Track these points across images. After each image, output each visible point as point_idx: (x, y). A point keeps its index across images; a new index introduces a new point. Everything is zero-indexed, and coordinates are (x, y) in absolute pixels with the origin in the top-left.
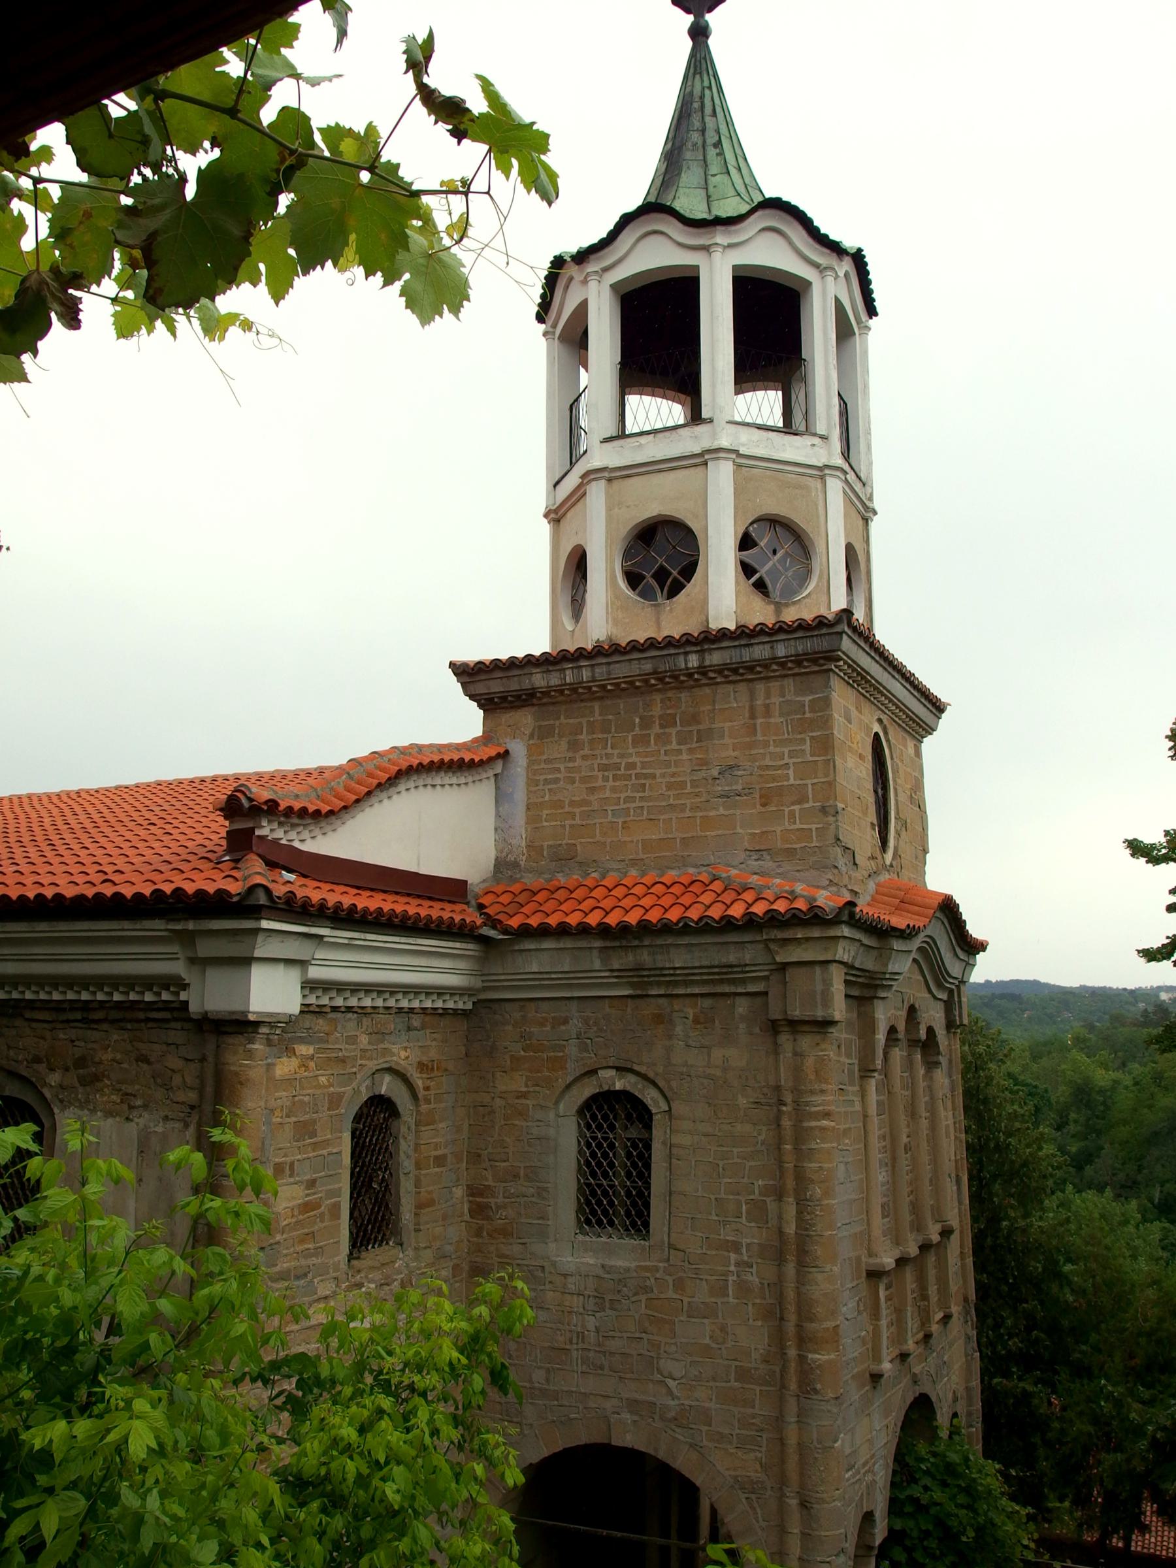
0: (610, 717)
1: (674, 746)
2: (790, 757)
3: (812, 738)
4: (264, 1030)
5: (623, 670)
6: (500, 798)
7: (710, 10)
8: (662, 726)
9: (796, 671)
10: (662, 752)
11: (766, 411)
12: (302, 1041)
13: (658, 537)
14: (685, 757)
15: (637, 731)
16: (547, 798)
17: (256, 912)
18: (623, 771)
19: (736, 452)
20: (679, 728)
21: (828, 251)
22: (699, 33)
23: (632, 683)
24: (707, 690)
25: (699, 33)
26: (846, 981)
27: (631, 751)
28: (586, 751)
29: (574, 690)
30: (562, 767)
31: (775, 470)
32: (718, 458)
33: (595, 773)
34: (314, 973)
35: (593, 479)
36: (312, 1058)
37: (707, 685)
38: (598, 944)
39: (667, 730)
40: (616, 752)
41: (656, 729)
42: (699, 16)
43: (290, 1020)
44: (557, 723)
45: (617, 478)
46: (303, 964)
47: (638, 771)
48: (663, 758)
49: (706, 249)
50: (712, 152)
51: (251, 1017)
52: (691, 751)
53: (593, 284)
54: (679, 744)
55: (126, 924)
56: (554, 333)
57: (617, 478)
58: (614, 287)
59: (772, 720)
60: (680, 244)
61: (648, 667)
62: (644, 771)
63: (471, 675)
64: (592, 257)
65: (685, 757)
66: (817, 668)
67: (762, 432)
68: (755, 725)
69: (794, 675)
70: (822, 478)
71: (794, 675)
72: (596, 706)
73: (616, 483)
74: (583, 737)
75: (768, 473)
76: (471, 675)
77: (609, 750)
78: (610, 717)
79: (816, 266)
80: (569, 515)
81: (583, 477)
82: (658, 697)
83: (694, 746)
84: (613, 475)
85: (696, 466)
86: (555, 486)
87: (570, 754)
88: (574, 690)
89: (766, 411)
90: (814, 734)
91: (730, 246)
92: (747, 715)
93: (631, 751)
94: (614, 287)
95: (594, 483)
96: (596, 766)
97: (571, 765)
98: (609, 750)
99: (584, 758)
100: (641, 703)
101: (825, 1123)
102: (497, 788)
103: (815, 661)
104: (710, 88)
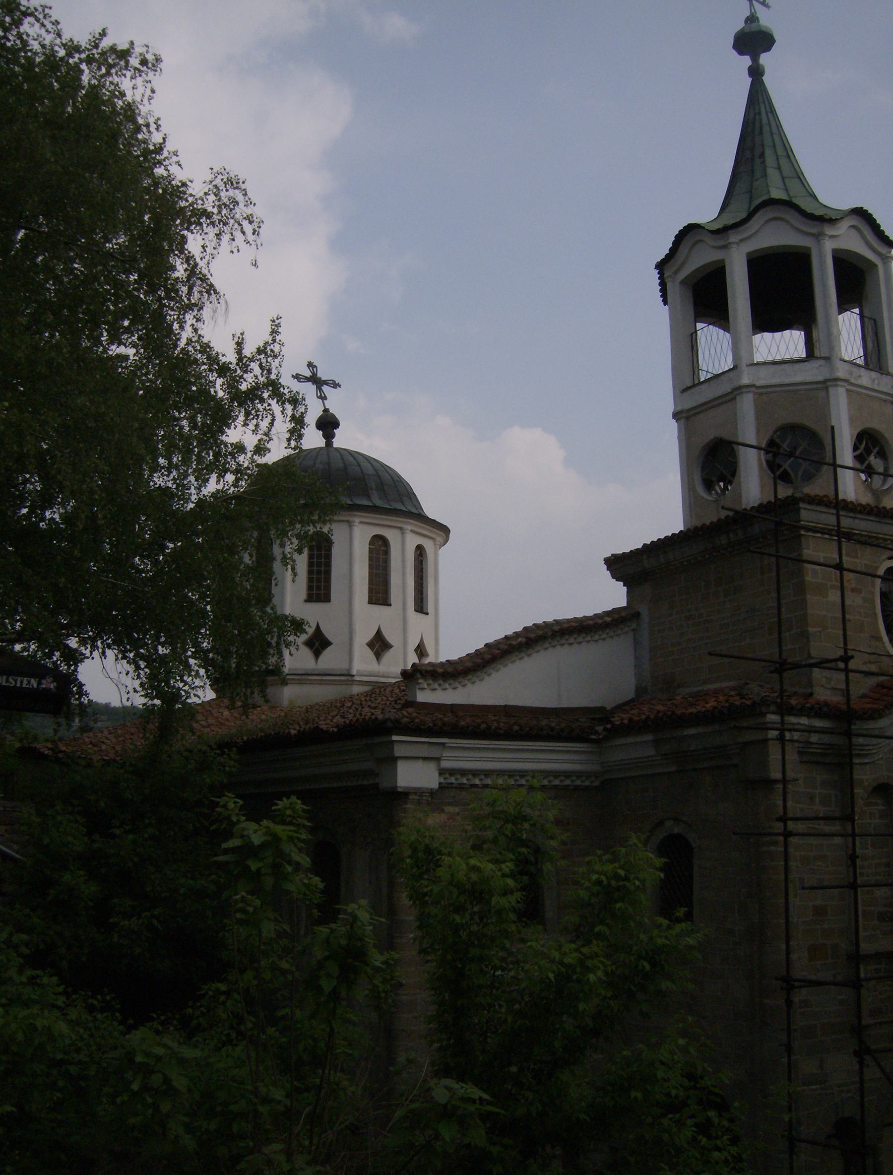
4: (411, 797)
6: (637, 643)
11: (792, 347)
12: (450, 804)
16: (659, 642)
17: (390, 732)
19: (753, 386)
22: (756, 72)
25: (756, 72)
26: (799, 753)
32: (741, 393)
34: (445, 764)
36: (458, 814)
38: (649, 737)
42: (755, 59)
43: (432, 793)
45: (691, 416)
46: (438, 760)
50: (758, 161)
51: (399, 790)
55: (530, 743)
58: (684, 282)
60: (714, 247)
63: (617, 565)
67: (777, 366)
70: (827, 388)
76: (617, 565)
79: (813, 235)
89: (792, 347)
91: (741, 241)
101: (773, 848)
102: (635, 639)
104: (760, 113)
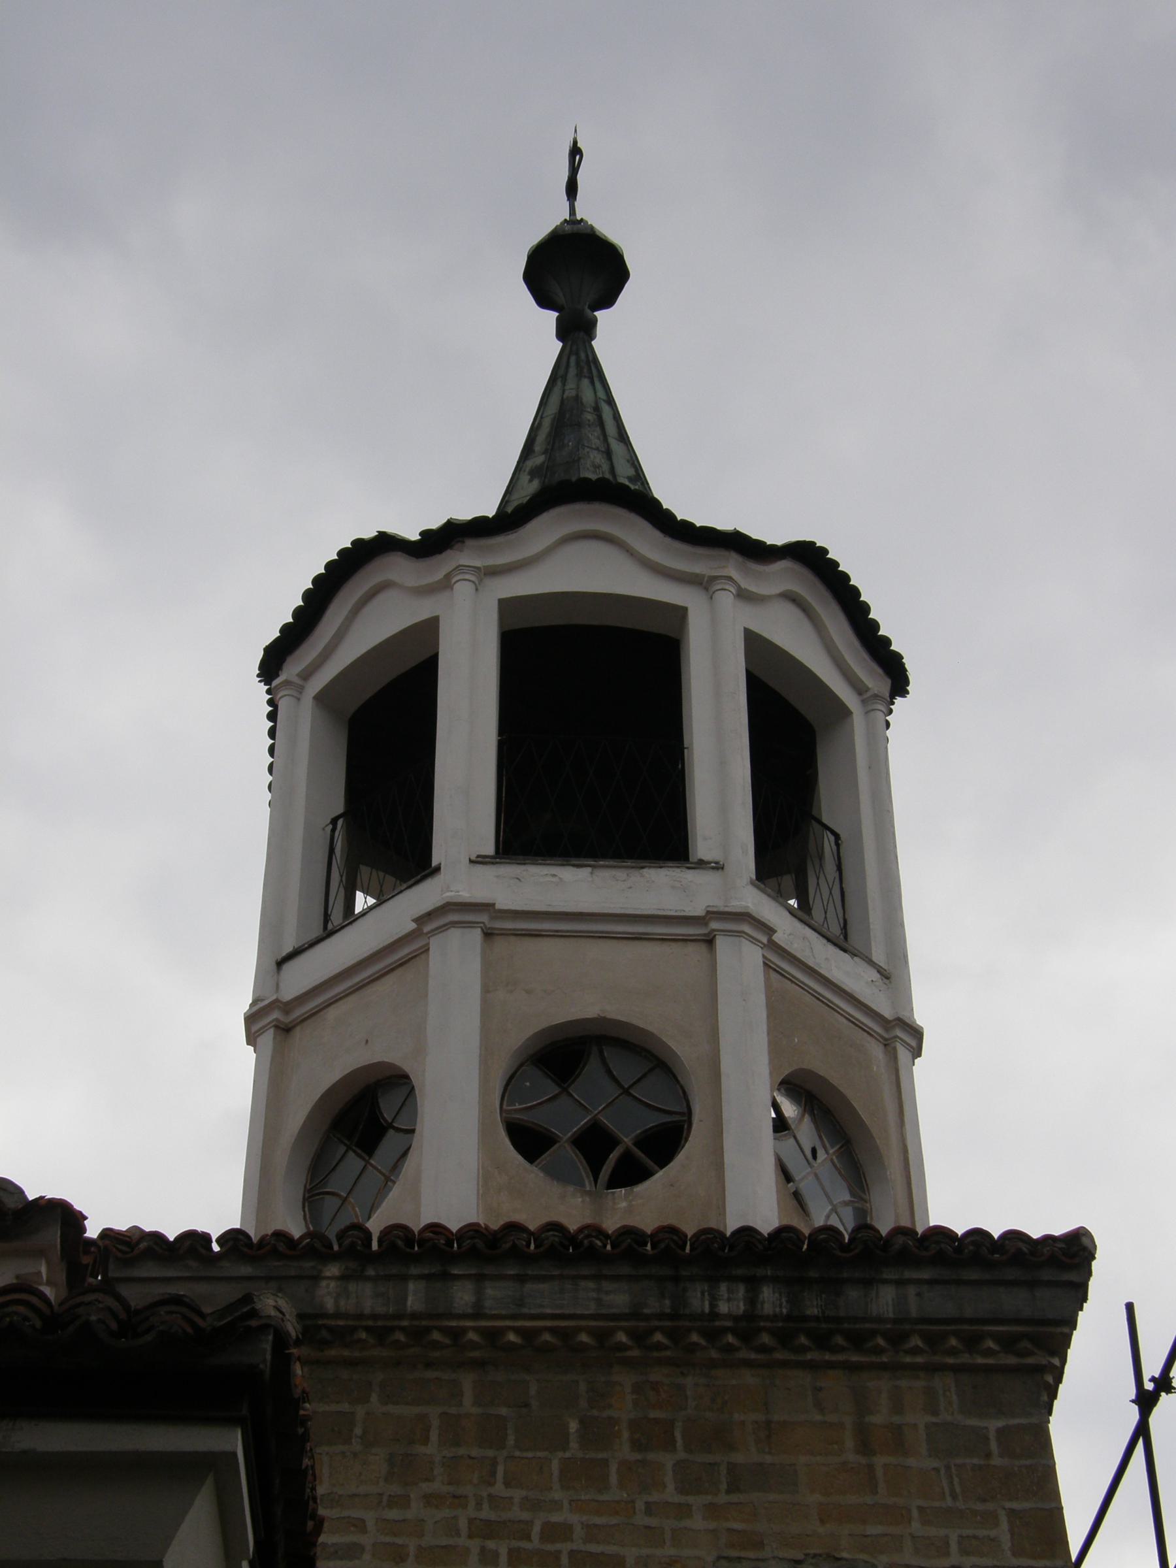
0: (504, 1411)
1: (670, 1494)
2: (964, 1552)
3: (1012, 1513)
5: (551, 1298)
7: (558, 320)
8: (636, 1445)
9: (965, 1358)
10: (640, 1505)
13: (592, 1069)
14: (698, 1523)
15: (574, 1449)
18: (535, 1543)
20: (681, 1455)
21: (880, 671)
23: (565, 1335)
24: (749, 1378)
27: (557, 1495)
28: (438, 1486)
29: (418, 1335)
30: (370, 1517)
31: (818, 998)
33: (462, 1541)
35: (454, 924)
37: (748, 1364)
39: (651, 1456)
40: (517, 1494)
41: (624, 1451)
44: (360, 1411)
45: (505, 933)
47: (577, 1545)
48: (641, 1520)
49: (704, 584)
52: (712, 1511)
53: (463, 589)
54: (682, 1490)
56: (301, 689)
57: (505, 933)
59: (911, 1462)
61: (619, 1298)
62: (594, 1548)
64: (471, 543)
65: (698, 1523)
66: (1012, 1360)
68: (871, 1468)
69: (957, 1369)
71: (957, 1369)
72: (467, 1381)
73: (500, 945)
74: (432, 1449)
75: (808, 998)
77: (499, 1488)
78: (504, 1411)
80: (332, 1013)
81: (421, 920)
82: (625, 1379)
83: (722, 1498)
84: (499, 924)
85: (685, 940)
86: (280, 964)
87: (395, 1489)
88: (418, 1335)
90: (1015, 1505)
92: (849, 1443)
93: (557, 1495)
94: (507, 607)
95: (455, 934)
96: (463, 1524)
97: (393, 1514)
98: (499, 1488)
99: (430, 1500)
100: (583, 1387)
103: (1009, 1343)
